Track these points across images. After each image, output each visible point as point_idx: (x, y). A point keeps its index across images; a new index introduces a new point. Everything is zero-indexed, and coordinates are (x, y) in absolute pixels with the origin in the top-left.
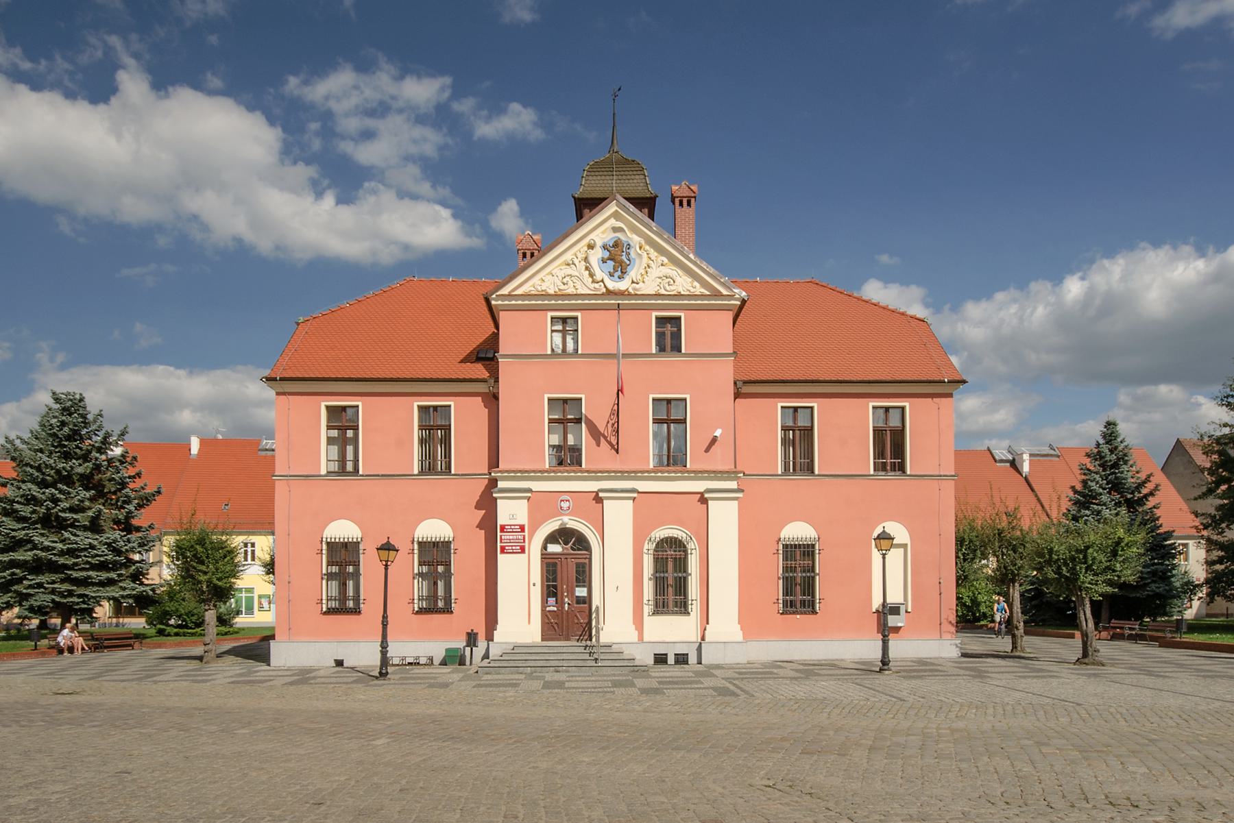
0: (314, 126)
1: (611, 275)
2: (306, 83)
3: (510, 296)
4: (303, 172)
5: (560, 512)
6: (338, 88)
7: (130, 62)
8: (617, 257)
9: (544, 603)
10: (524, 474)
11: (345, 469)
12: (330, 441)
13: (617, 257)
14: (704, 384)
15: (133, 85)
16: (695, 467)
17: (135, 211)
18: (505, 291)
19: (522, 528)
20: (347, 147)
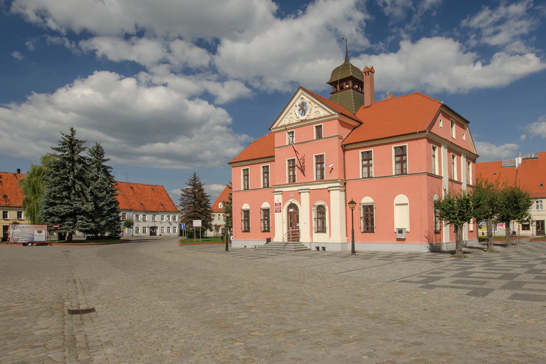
0: (473, 36)
1: (301, 115)
2: (470, 20)
3: (276, 128)
4: (472, 55)
5: (290, 198)
6: (483, 18)
7: (404, 36)
8: (303, 108)
9: (288, 229)
10: (280, 186)
11: (403, 172)
12: (396, 162)
13: (303, 108)
14: (331, 149)
15: (405, 45)
16: (327, 179)
17: (405, 87)
18: (274, 126)
19: (280, 204)
20: (486, 40)
